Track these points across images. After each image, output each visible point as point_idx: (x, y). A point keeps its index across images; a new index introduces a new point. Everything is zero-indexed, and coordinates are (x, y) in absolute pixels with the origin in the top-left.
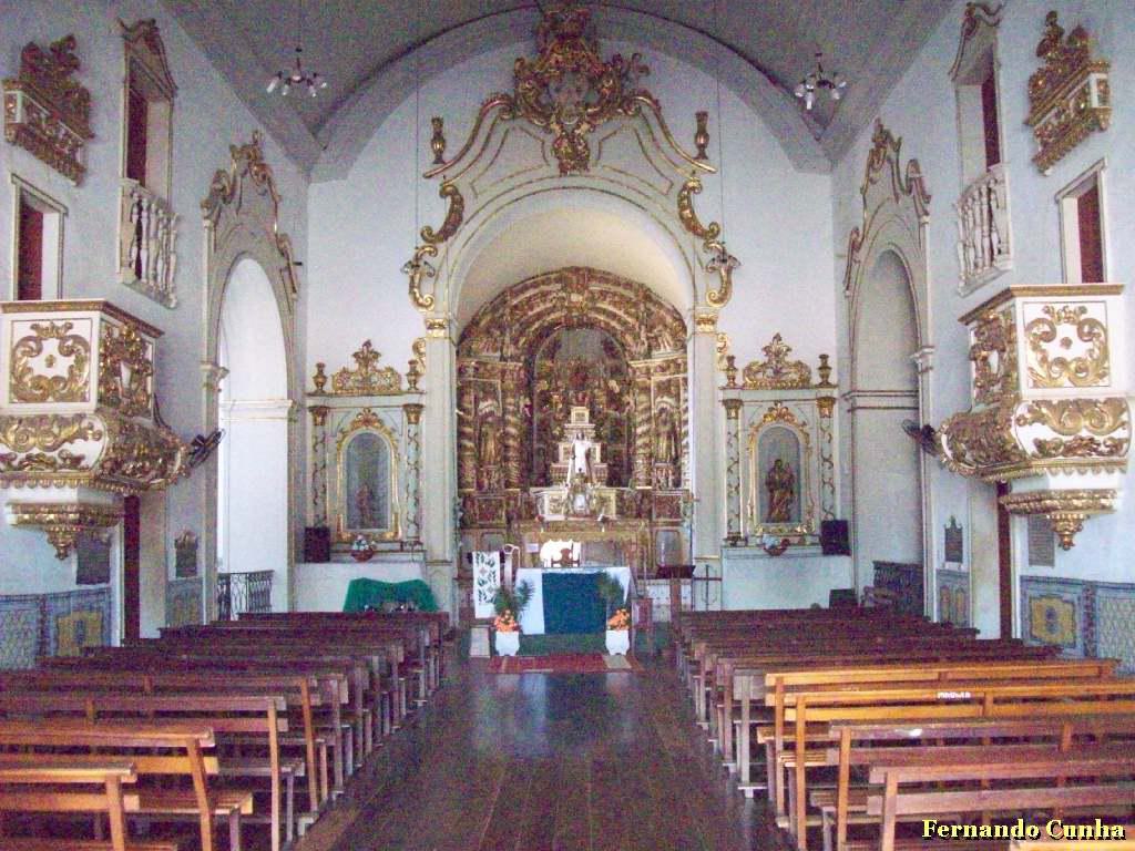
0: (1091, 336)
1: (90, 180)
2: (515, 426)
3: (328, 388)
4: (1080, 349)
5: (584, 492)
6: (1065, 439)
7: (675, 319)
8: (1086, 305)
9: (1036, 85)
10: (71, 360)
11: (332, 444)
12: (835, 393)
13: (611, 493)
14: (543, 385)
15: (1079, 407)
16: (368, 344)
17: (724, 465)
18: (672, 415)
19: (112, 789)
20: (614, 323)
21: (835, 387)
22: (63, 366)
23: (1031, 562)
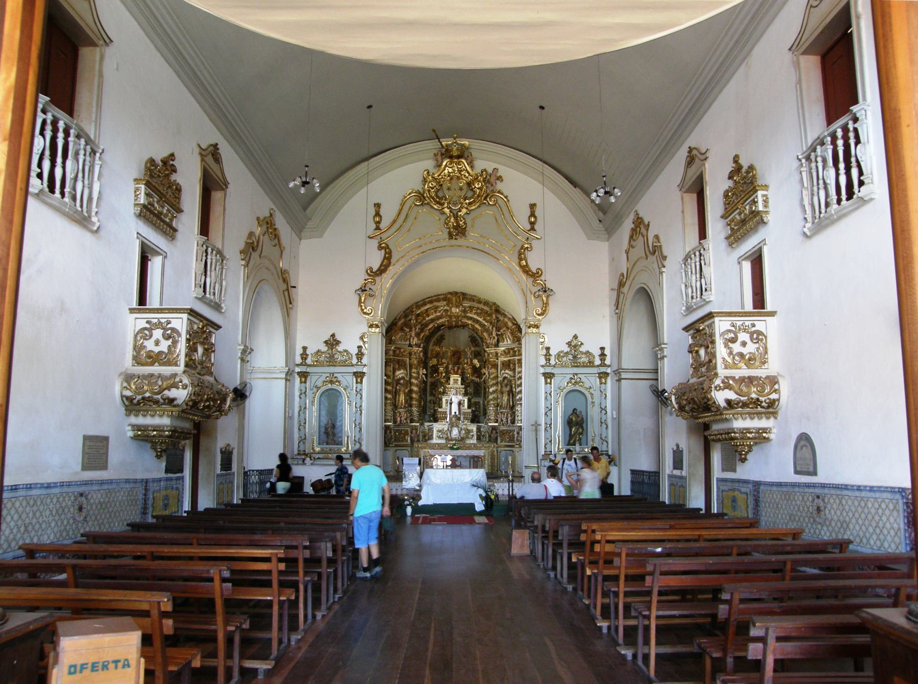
0: (758, 340)
1: (179, 235)
2: (417, 386)
3: (309, 361)
4: (751, 348)
5: (457, 426)
6: (742, 398)
7: (514, 324)
9: (728, 195)
10: (169, 342)
12: (609, 370)
13: (473, 427)
15: (751, 380)
16: (333, 335)
17: (543, 411)
18: (511, 381)
19: (274, 560)
20: (477, 326)
21: (609, 366)
22: (164, 346)
23: (723, 470)
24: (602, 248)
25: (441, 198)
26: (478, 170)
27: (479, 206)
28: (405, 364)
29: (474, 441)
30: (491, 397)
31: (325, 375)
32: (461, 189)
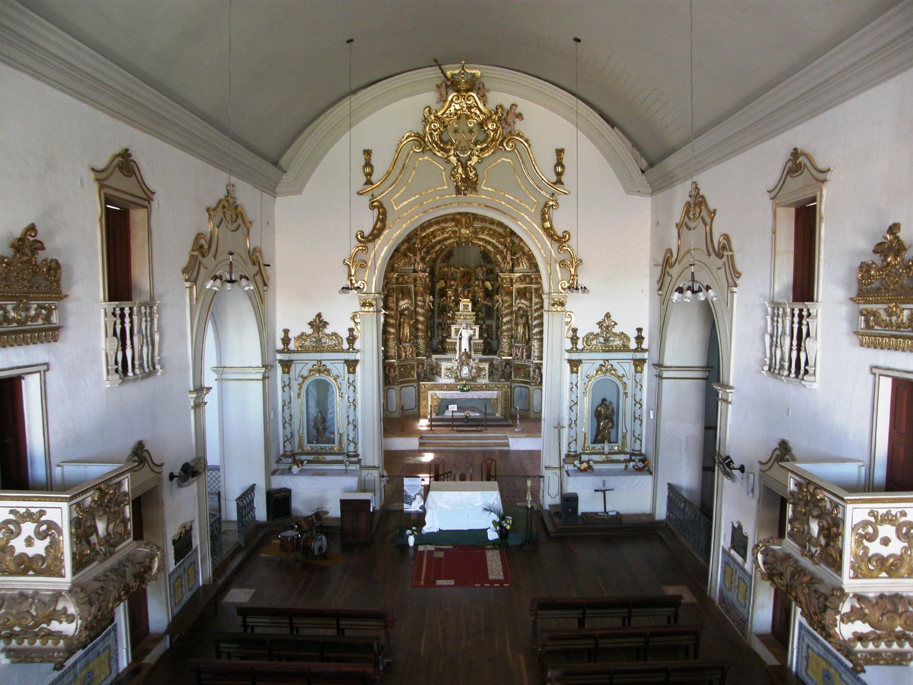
2: (423, 315)
3: (292, 346)
5: (468, 365)
8: (906, 510)
10: (47, 542)
11: (295, 385)
14: (441, 284)
16: (319, 316)
18: (527, 311)
22: (40, 547)
24: (642, 209)
25: (446, 143)
26: (492, 106)
27: (493, 153)
28: (410, 292)
29: (485, 381)
30: (504, 328)
31: (311, 363)
32: (471, 131)
